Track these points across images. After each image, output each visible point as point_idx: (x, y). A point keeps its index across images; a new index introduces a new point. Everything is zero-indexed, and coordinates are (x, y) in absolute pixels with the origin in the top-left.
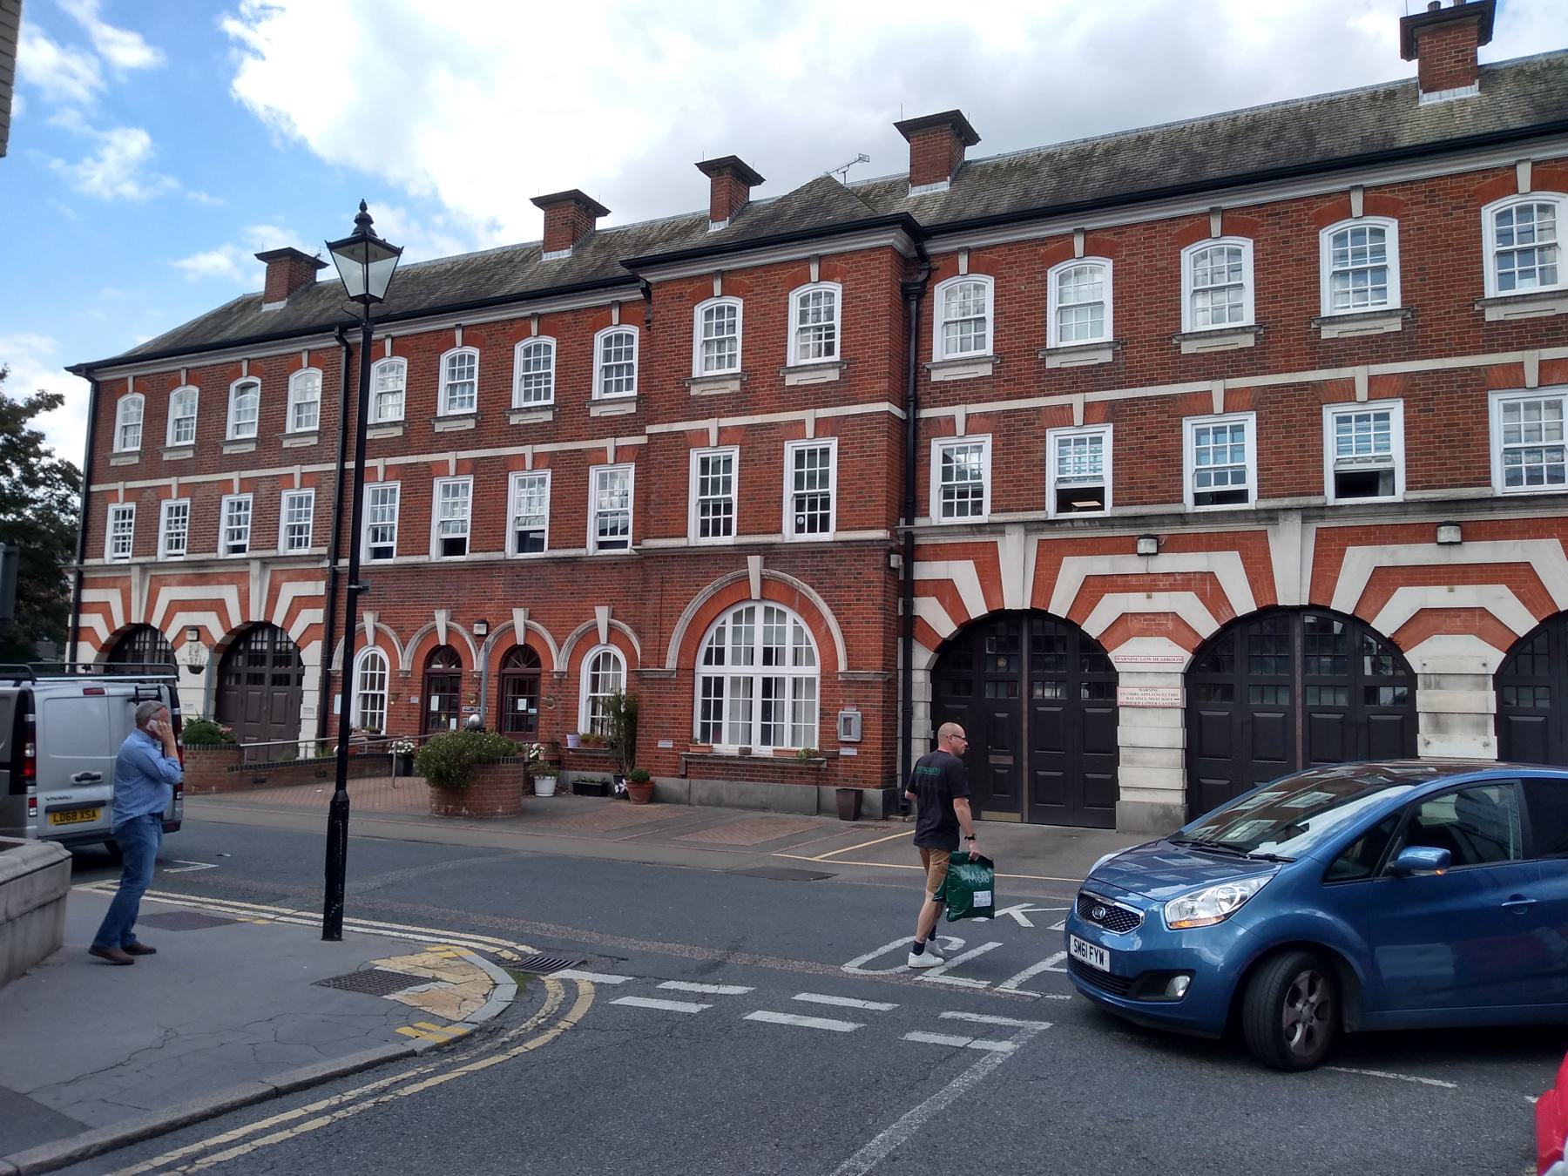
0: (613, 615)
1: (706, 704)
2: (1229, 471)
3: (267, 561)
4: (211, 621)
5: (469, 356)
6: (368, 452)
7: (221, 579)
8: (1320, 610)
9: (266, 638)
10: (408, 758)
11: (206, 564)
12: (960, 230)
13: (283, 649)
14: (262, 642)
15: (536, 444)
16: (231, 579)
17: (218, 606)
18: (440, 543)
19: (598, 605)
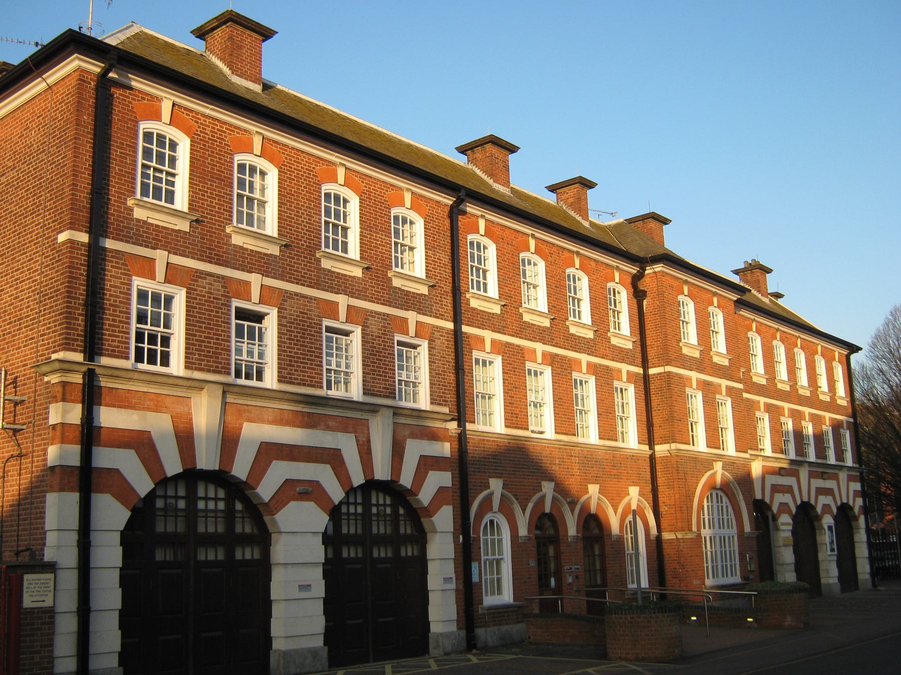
0: (505, 486)
1: (716, 562)
2: (146, 333)
3: (401, 411)
4: (324, 475)
5: (158, 135)
6: (650, 364)
7: (331, 423)
8: (163, 482)
9: (359, 500)
10: (698, 609)
11: (324, 402)
12: (808, 330)
13: (184, 514)
14: (356, 504)
15: (267, 276)
16: (345, 426)
17: (334, 458)
18: (263, 380)
19: (590, 483)
